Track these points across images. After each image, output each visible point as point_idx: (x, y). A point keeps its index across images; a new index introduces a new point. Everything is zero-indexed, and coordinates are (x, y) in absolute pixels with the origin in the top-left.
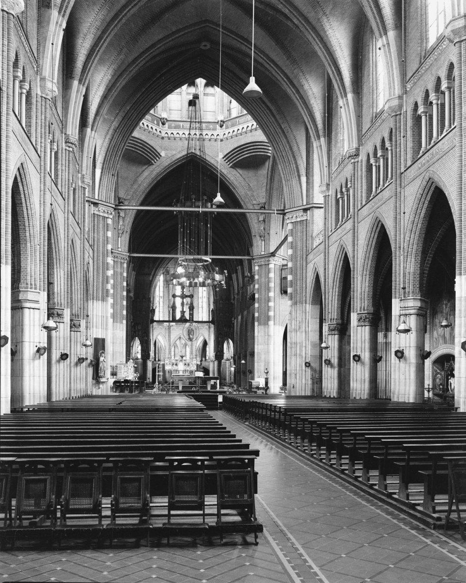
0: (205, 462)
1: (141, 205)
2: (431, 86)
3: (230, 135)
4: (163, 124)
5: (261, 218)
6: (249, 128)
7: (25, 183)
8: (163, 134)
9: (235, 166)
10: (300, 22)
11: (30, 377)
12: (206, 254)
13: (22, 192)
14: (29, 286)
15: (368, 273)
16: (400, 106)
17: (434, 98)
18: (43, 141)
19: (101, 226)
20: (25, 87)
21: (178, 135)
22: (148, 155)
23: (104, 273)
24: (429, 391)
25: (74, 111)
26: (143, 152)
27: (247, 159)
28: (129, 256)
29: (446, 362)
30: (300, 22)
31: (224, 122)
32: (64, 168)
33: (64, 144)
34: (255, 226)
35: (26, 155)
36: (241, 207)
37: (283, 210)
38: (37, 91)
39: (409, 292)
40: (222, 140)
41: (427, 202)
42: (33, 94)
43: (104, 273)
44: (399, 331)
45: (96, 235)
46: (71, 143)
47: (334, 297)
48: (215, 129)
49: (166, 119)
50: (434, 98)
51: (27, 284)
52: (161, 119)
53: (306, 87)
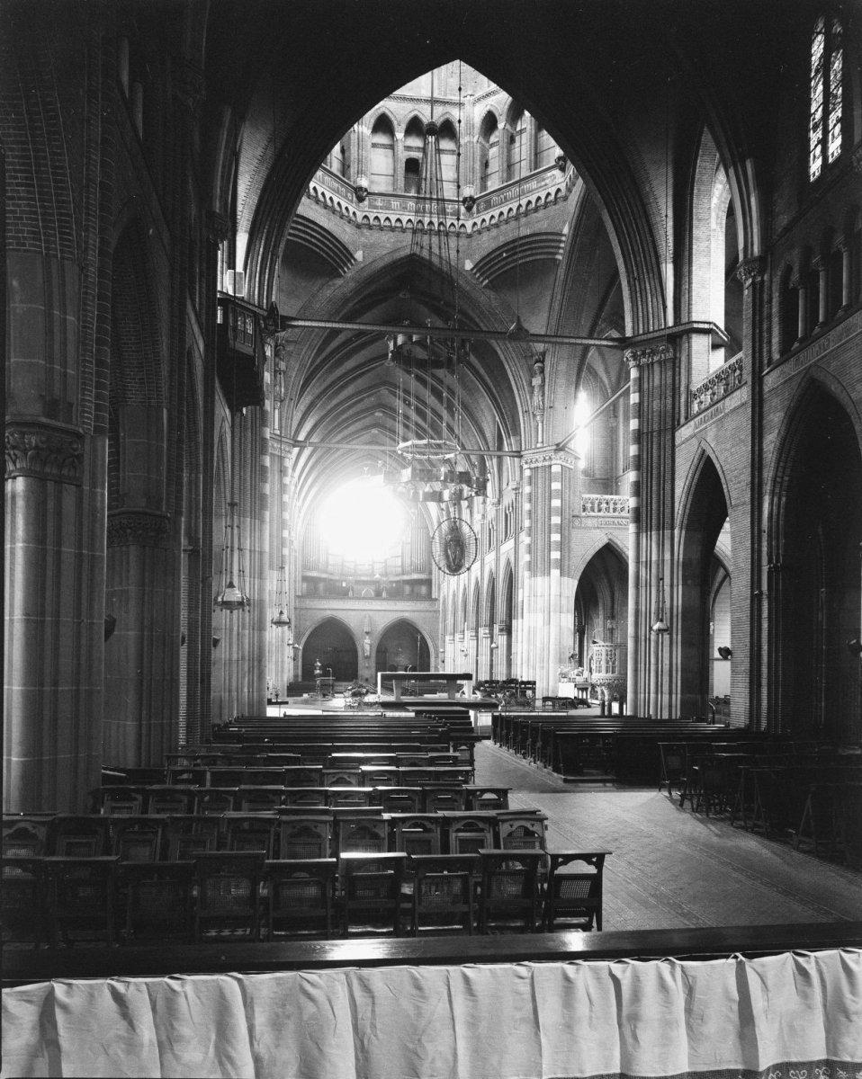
0: (7, 870)
4: (361, 199)
6: (523, 210)
8: (359, 219)
12: (469, 717)
29: (505, 903)
37: (519, 452)
49: (366, 190)
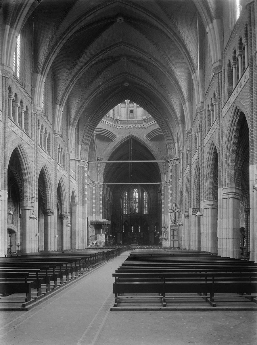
1: (109, 160)
2: (212, 96)
3: (149, 125)
4: (118, 122)
5: (164, 164)
7: (23, 153)
8: (118, 127)
9: (152, 140)
10: (163, 70)
11: (29, 241)
13: (22, 157)
14: (28, 199)
15: (196, 189)
16: (203, 107)
17: (214, 101)
18: (35, 133)
19: (82, 171)
20: (23, 109)
21: (122, 127)
22: (110, 137)
23: (83, 193)
24: (18, 247)
25: (58, 119)
26: (108, 135)
27: (156, 137)
28: (103, 184)
30: (163, 70)
31: (146, 119)
32: (53, 145)
33: (53, 134)
34: (162, 168)
35: (22, 140)
36: (155, 159)
38: (31, 111)
39: (207, 197)
40: (145, 128)
41: (213, 153)
42: (29, 112)
43: (83, 193)
44: (30, 218)
45: (79, 176)
46: (57, 134)
47: (186, 201)
48: (142, 123)
50: (214, 101)
51: (27, 199)
52: (116, 120)
53: (172, 101)
